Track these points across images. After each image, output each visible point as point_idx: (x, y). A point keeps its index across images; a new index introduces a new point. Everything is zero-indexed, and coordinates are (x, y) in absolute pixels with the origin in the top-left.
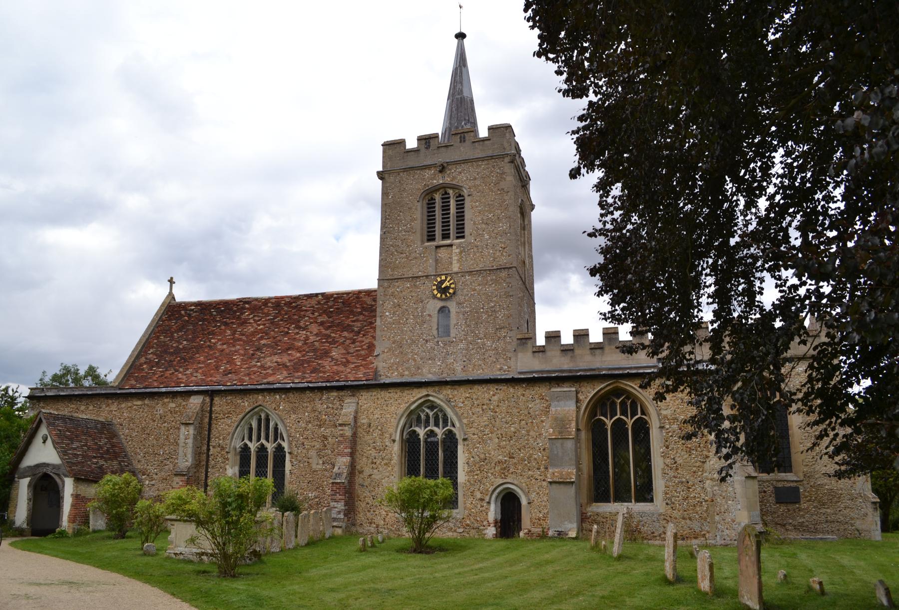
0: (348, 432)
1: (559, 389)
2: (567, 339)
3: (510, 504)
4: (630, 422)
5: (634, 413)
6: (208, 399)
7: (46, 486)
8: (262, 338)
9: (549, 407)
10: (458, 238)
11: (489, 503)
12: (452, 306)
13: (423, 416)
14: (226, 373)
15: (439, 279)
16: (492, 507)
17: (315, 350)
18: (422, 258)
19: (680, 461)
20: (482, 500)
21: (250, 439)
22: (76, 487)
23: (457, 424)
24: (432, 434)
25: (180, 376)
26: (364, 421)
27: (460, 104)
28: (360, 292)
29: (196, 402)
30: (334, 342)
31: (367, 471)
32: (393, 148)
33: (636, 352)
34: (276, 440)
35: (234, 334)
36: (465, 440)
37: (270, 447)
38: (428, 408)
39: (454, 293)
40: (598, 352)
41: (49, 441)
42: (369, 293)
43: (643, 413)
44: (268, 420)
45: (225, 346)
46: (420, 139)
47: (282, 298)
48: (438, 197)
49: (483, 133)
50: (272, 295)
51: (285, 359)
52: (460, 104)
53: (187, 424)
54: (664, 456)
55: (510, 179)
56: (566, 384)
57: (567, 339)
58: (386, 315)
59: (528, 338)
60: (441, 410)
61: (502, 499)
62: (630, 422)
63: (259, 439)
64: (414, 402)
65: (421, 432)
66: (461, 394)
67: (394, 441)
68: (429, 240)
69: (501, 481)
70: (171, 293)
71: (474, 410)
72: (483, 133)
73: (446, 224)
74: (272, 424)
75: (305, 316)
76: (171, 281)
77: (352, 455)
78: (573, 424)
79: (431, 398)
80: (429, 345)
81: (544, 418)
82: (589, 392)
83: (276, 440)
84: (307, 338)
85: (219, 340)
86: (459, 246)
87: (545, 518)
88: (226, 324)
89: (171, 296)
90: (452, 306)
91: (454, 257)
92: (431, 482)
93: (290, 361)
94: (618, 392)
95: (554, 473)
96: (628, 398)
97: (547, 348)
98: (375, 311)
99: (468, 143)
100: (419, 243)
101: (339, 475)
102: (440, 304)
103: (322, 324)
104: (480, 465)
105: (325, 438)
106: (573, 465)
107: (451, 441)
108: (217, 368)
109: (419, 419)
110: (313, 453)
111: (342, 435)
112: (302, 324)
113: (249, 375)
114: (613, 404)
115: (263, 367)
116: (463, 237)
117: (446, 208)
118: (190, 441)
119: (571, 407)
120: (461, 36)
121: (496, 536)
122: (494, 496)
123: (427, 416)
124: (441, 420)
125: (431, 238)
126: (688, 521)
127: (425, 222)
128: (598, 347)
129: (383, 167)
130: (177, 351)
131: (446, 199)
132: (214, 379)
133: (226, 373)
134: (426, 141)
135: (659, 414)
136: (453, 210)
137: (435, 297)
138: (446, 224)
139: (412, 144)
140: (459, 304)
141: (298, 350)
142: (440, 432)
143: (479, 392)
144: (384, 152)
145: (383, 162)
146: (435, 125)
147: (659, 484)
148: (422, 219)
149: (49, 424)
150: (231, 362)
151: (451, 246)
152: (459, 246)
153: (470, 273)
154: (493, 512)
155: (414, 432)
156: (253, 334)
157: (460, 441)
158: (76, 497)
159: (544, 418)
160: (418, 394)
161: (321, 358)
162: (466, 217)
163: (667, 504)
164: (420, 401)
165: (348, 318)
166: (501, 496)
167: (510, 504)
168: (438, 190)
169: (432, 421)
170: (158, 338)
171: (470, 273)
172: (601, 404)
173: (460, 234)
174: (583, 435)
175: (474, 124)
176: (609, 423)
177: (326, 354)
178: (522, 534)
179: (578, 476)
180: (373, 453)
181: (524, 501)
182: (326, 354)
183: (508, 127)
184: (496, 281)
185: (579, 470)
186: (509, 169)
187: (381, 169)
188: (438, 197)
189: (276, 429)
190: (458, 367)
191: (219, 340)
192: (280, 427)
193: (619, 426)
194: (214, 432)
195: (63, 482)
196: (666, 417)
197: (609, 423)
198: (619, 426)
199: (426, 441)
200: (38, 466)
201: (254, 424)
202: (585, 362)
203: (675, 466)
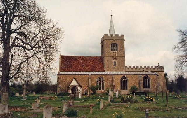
27: (111, 27)
33: (149, 67)
37: (101, 82)
46: (121, 35)
52: (111, 27)
66: (128, 75)
82: (144, 76)
90: (116, 61)
92: (100, 90)
94: (124, 77)
107: (127, 81)
120: (112, 16)
125: (112, 51)
130: (67, 65)
139: (120, 36)
143: (131, 75)
147: (151, 86)
160: (122, 76)
172: (145, 77)
173: (116, 50)
177: (95, 67)
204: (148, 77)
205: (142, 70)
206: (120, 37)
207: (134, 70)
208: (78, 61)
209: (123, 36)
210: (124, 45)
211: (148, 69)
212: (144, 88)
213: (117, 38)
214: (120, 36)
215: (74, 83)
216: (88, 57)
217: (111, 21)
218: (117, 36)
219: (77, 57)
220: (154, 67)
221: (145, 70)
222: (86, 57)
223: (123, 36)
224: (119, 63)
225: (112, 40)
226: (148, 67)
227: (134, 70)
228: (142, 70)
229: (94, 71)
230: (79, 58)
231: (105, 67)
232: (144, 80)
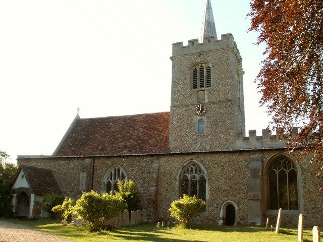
0: (155, 176)
1: (254, 156)
2: (259, 134)
3: (230, 209)
4: (287, 172)
7: (23, 195)
8: (118, 134)
9: (249, 164)
10: (208, 87)
11: (220, 209)
12: (205, 118)
13: (190, 169)
14: (102, 150)
15: (204, 112)
16: (222, 211)
17: (141, 140)
19: (311, 190)
20: (217, 208)
21: (111, 179)
22: (35, 198)
23: (206, 172)
24: (194, 177)
25: (81, 151)
26: (162, 171)
27: (210, 25)
28: (162, 113)
29: (88, 161)
30: (150, 136)
31: (164, 194)
32: (177, 46)
35: (105, 132)
36: (209, 180)
38: (192, 165)
39: (206, 112)
40: (274, 139)
41: (24, 177)
42: (166, 113)
43: (294, 167)
44: (119, 170)
45: (101, 138)
46: (189, 41)
49: (219, 38)
50: (123, 115)
51: (128, 144)
52: (210, 25)
53: (83, 171)
54: (304, 187)
55: (232, 59)
56: (257, 153)
57: (259, 134)
59: (241, 133)
60: (199, 166)
61: (227, 206)
62: (287, 172)
63: (115, 179)
64: (186, 162)
65: (189, 176)
66: (207, 158)
67: (176, 180)
68: (194, 88)
69: (225, 199)
71: (213, 166)
72: (219, 38)
73: (202, 80)
74: (121, 172)
75: (137, 124)
76: (78, 109)
77: (157, 186)
78: (260, 172)
79: (193, 160)
80: (194, 137)
81: (246, 170)
82: (268, 157)
85: (99, 135)
87: (247, 216)
88: (102, 128)
89: (78, 116)
91: (206, 95)
93: (130, 145)
94: (282, 157)
95: (251, 194)
96: (287, 160)
97: (251, 138)
98: (169, 121)
99: (212, 43)
100: (189, 89)
101: (150, 195)
102: (199, 118)
103: (145, 128)
104: (216, 191)
105: (145, 178)
106: (259, 187)
107: (203, 180)
108: (98, 148)
111: (152, 177)
113: (111, 151)
115: (118, 147)
116: (210, 86)
118: (84, 179)
119: (259, 164)
121: (223, 224)
122: (222, 206)
124: (198, 171)
125: (195, 87)
126: (315, 219)
127: (192, 80)
129: (173, 55)
132: (96, 153)
133: (102, 150)
134: (193, 42)
135: (301, 168)
136: (205, 74)
137: (197, 114)
138: (202, 80)
140: (208, 118)
141: (134, 139)
142: (198, 177)
143: (217, 158)
144: (173, 48)
145: (173, 52)
146: (200, 37)
148: (191, 79)
149: (24, 170)
150: (104, 145)
151: (204, 90)
152: (208, 90)
153: (214, 103)
154: (222, 213)
155: (186, 176)
156: (114, 132)
157: (207, 180)
158: (36, 202)
159: (246, 170)
160: (187, 159)
161: (144, 143)
162: (211, 77)
163: (305, 210)
164: (188, 162)
165: (157, 125)
166: (227, 205)
167: (230, 209)
168: (198, 65)
169: (194, 171)
171: (214, 103)
172: (274, 163)
173: (209, 85)
174: (265, 177)
175: (215, 33)
176: (277, 172)
178: (235, 224)
179: (263, 197)
180: (166, 185)
181: (236, 208)
182: (146, 141)
183: (230, 35)
184: (225, 107)
185: (263, 194)
186: (231, 54)
189: (123, 174)
190: (208, 148)
191: (99, 135)
192: (124, 173)
193: (282, 174)
194: (95, 176)
196: (305, 169)
197: (277, 172)
198: (282, 174)
199: (191, 180)
200: (20, 188)
201: (113, 172)
202: (268, 144)
203: (309, 192)
204: (288, 162)
213: (211, 46)
218: (209, 41)
225: (193, 54)
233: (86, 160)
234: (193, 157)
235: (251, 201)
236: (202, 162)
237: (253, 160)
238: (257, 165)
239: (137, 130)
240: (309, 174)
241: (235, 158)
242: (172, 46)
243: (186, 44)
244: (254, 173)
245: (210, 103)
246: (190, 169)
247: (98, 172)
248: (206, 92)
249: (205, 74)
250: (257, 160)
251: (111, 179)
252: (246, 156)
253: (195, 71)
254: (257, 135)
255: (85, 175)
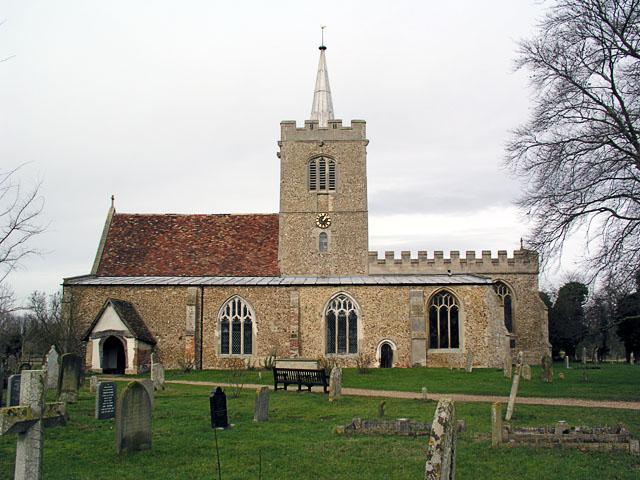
4: (449, 308)
5: (451, 303)
6: (200, 290)
13: (337, 303)
18: (310, 201)
21: (228, 315)
27: (324, 90)
28: (255, 215)
32: (287, 125)
34: (245, 315)
37: (242, 319)
44: (239, 303)
47: (200, 215)
48: (317, 161)
52: (324, 90)
58: (285, 232)
63: (234, 314)
65: (337, 312)
69: (382, 338)
70: (112, 207)
73: (322, 179)
82: (431, 291)
83: (245, 315)
84: (225, 246)
86: (332, 195)
90: (328, 232)
92: (225, 355)
103: (234, 236)
104: (371, 329)
107: (353, 318)
109: (334, 305)
110: (271, 323)
112: (219, 235)
114: (441, 299)
117: (323, 169)
120: (323, 48)
123: (340, 303)
125: (313, 188)
128: (415, 262)
130: (131, 251)
131: (322, 164)
136: (327, 171)
138: (322, 179)
139: (346, 124)
142: (347, 312)
147: (463, 339)
152: (332, 195)
154: (378, 355)
156: (185, 241)
170: (113, 240)
172: (436, 298)
173: (332, 183)
177: (242, 257)
187: (280, 139)
188: (317, 161)
193: (444, 310)
195: (126, 341)
197: (439, 308)
198: (444, 310)
204: (451, 299)
205: (442, 268)
206: (348, 129)
207: (408, 268)
208: (176, 232)
209: (359, 124)
210: (364, 164)
211: (485, 262)
212: (433, 344)
213: (335, 134)
214: (346, 124)
215: (111, 322)
216: (220, 216)
217: (323, 71)
218: (335, 127)
219: (174, 217)
220: (495, 256)
221: (455, 267)
222: (211, 217)
223: (359, 124)
224: (342, 241)
225: (312, 142)
226: (468, 253)
227: (423, 268)
228: (442, 268)
229: (231, 274)
230: (185, 220)
231: (282, 255)
232: (432, 312)
233: (89, 273)
234: (343, 288)
235: (415, 341)
236: (353, 295)
237: (414, 294)
238: (414, 300)
239: (222, 239)
240: (472, 311)
241: (393, 291)
242: (280, 127)
243: (300, 124)
244: (417, 309)
245: (335, 212)
246: (337, 303)
247: (209, 306)
248: (331, 198)
249: (327, 171)
250: (418, 294)
251: (240, 314)
252: (405, 290)
253: (313, 168)
254: (396, 258)
255: (194, 310)
